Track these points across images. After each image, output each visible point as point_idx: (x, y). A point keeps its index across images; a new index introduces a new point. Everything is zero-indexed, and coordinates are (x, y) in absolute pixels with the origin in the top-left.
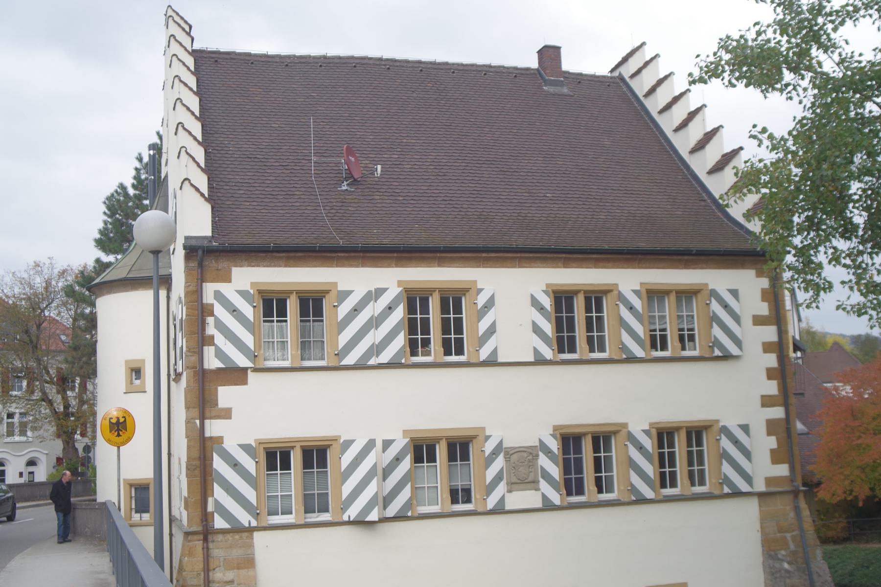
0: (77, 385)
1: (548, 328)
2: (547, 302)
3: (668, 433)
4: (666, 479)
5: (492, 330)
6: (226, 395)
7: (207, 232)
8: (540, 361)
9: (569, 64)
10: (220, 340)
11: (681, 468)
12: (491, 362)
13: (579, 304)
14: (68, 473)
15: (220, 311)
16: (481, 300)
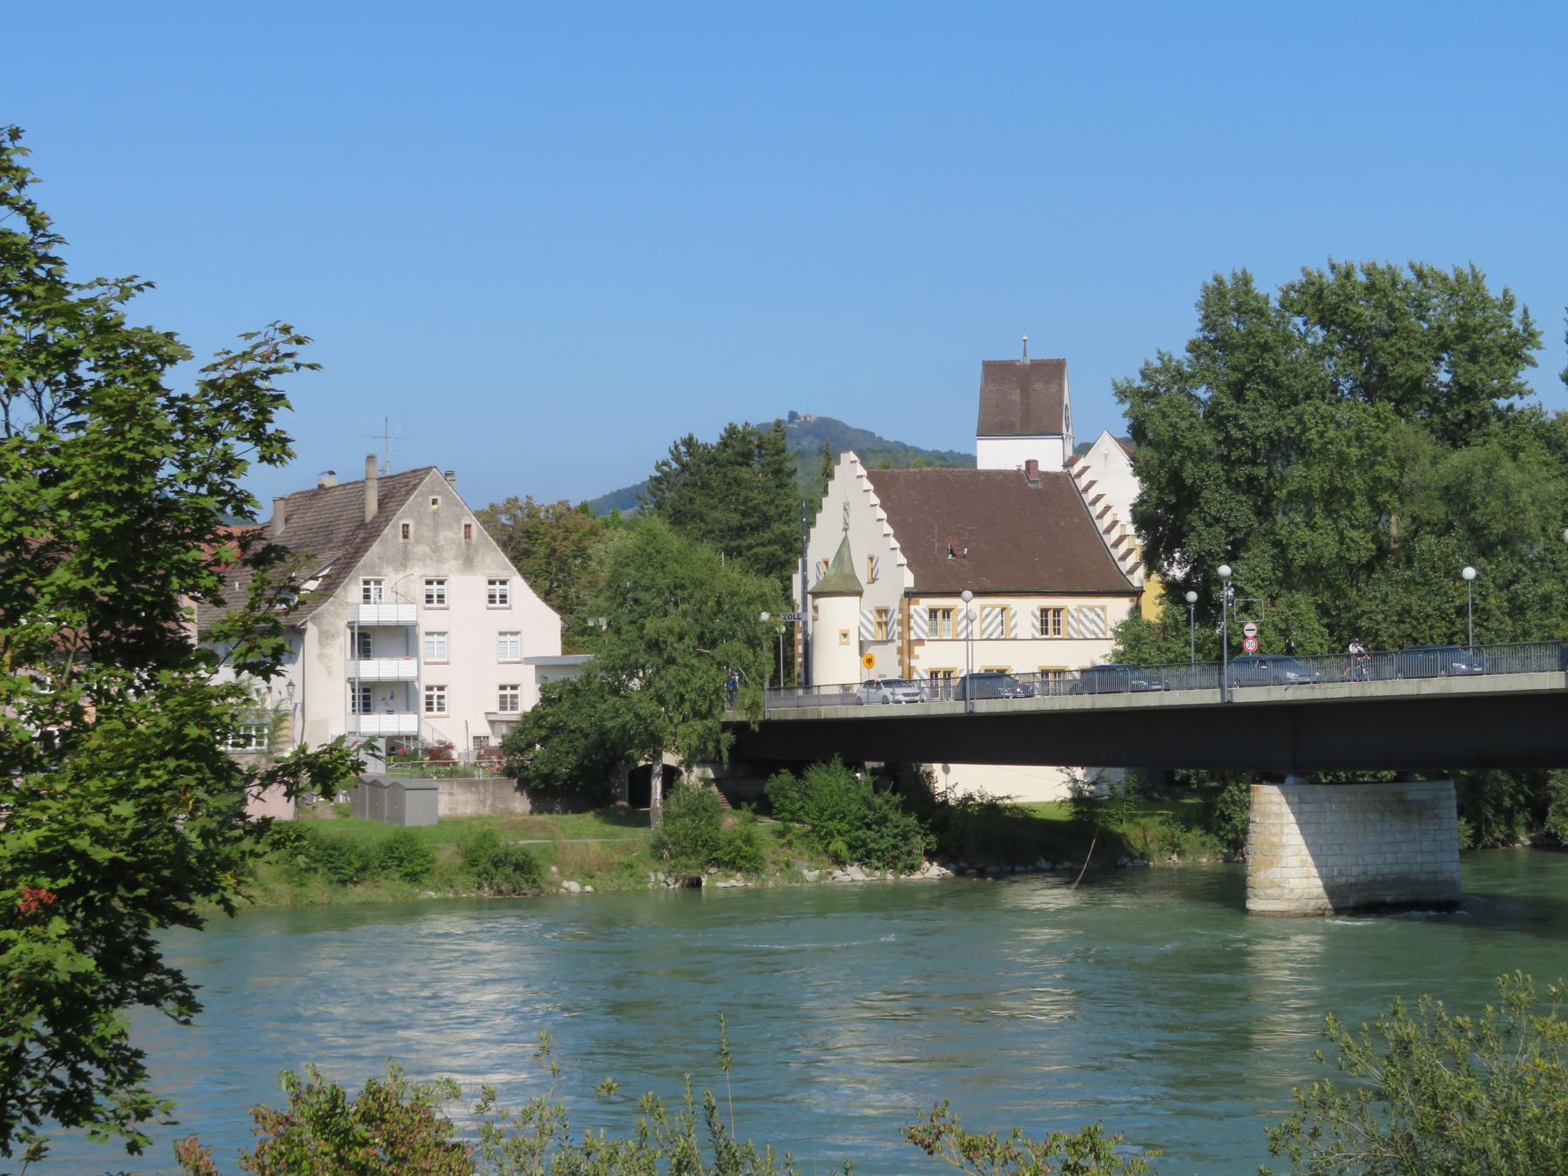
0: (1188, 861)
1: (1038, 624)
2: (1038, 614)
3: (1055, 610)
4: (1044, 631)
5: (1015, 626)
6: (917, 650)
7: (912, 585)
8: (1034, 639)
9: (1041, 468)
10: (916, 628)
11: (1051, 626)
12: (1014, 639)
13: (1050, 614)
14: (784, 629)
15: (915, 616)
16: (1012, 613)
